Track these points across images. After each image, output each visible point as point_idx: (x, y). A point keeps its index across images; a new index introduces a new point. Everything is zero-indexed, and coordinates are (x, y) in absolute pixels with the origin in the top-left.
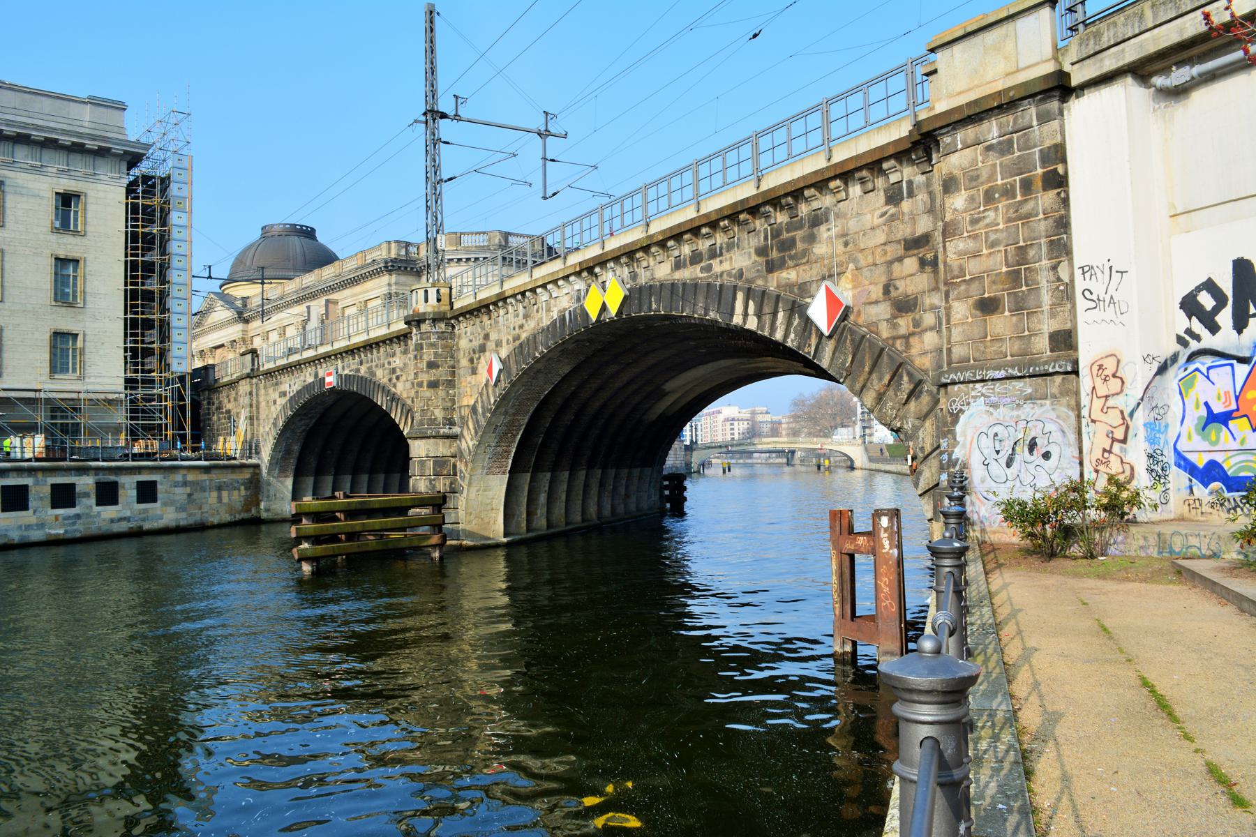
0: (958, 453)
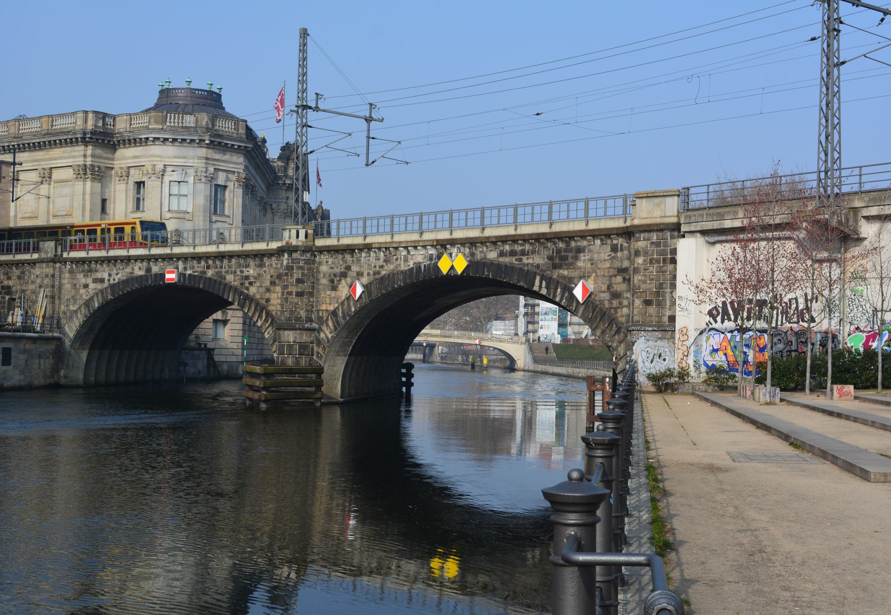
0: (633, 357)
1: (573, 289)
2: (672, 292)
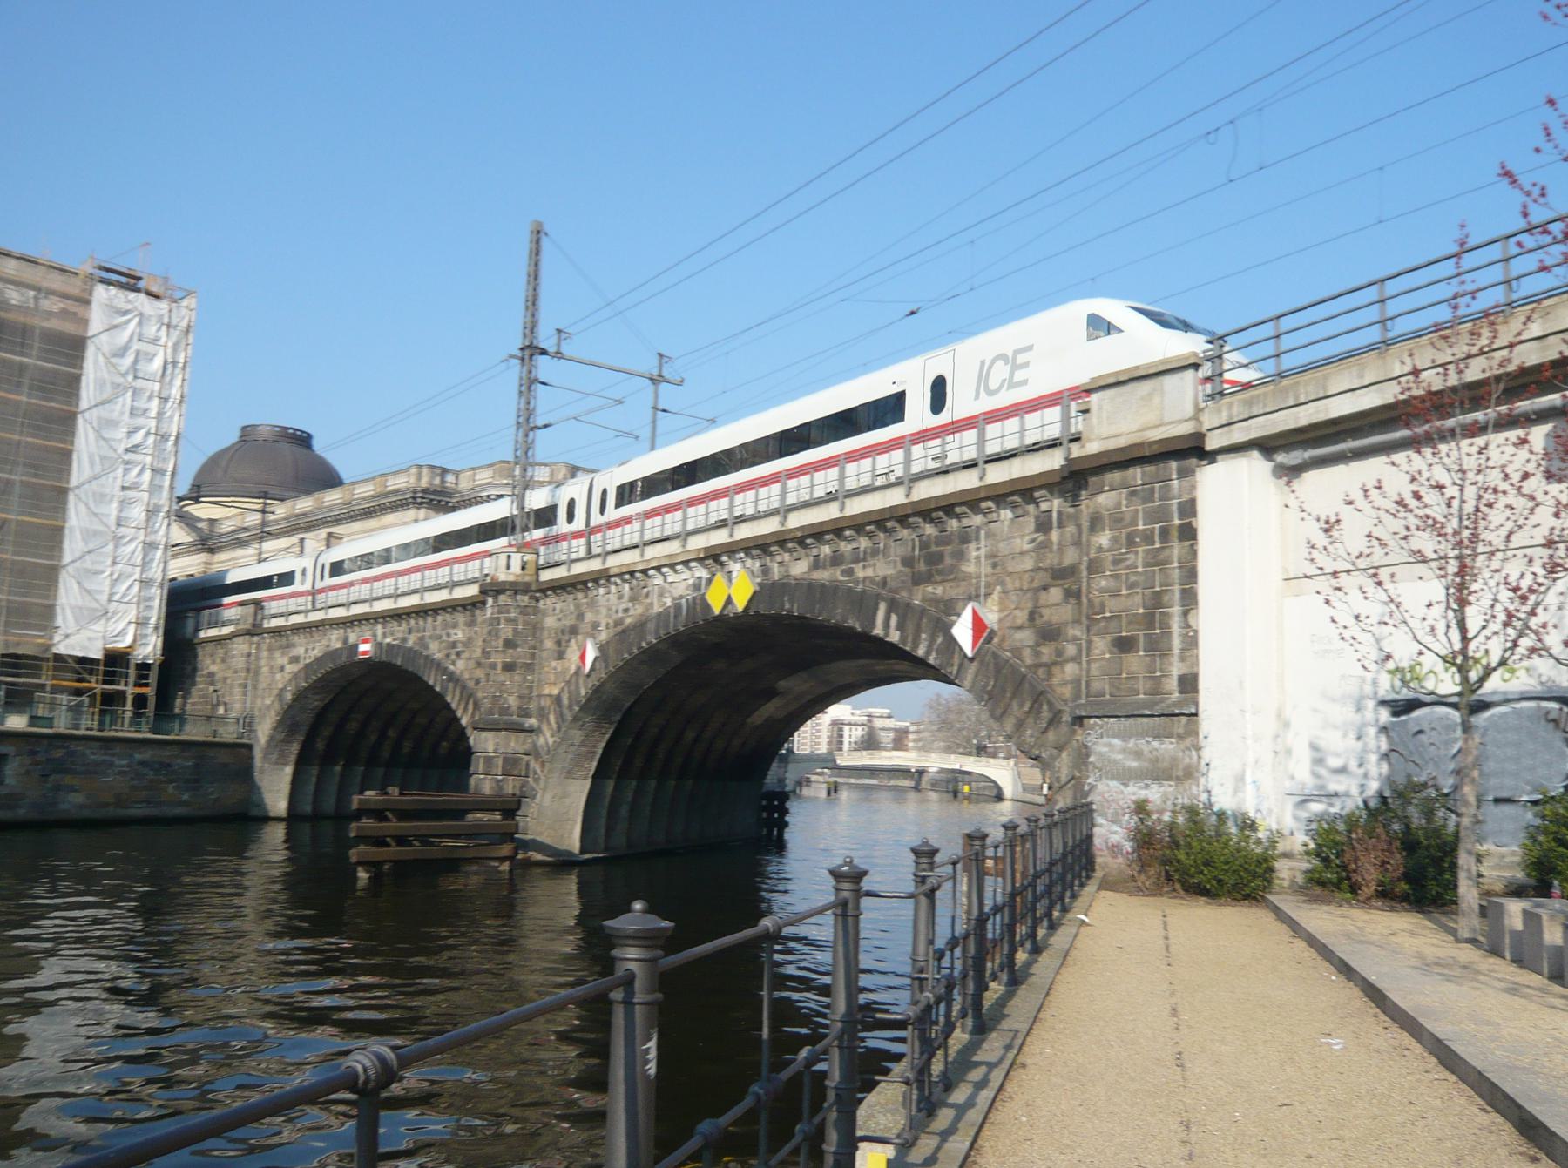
1: (952, 624)
2: (1185, 614)
